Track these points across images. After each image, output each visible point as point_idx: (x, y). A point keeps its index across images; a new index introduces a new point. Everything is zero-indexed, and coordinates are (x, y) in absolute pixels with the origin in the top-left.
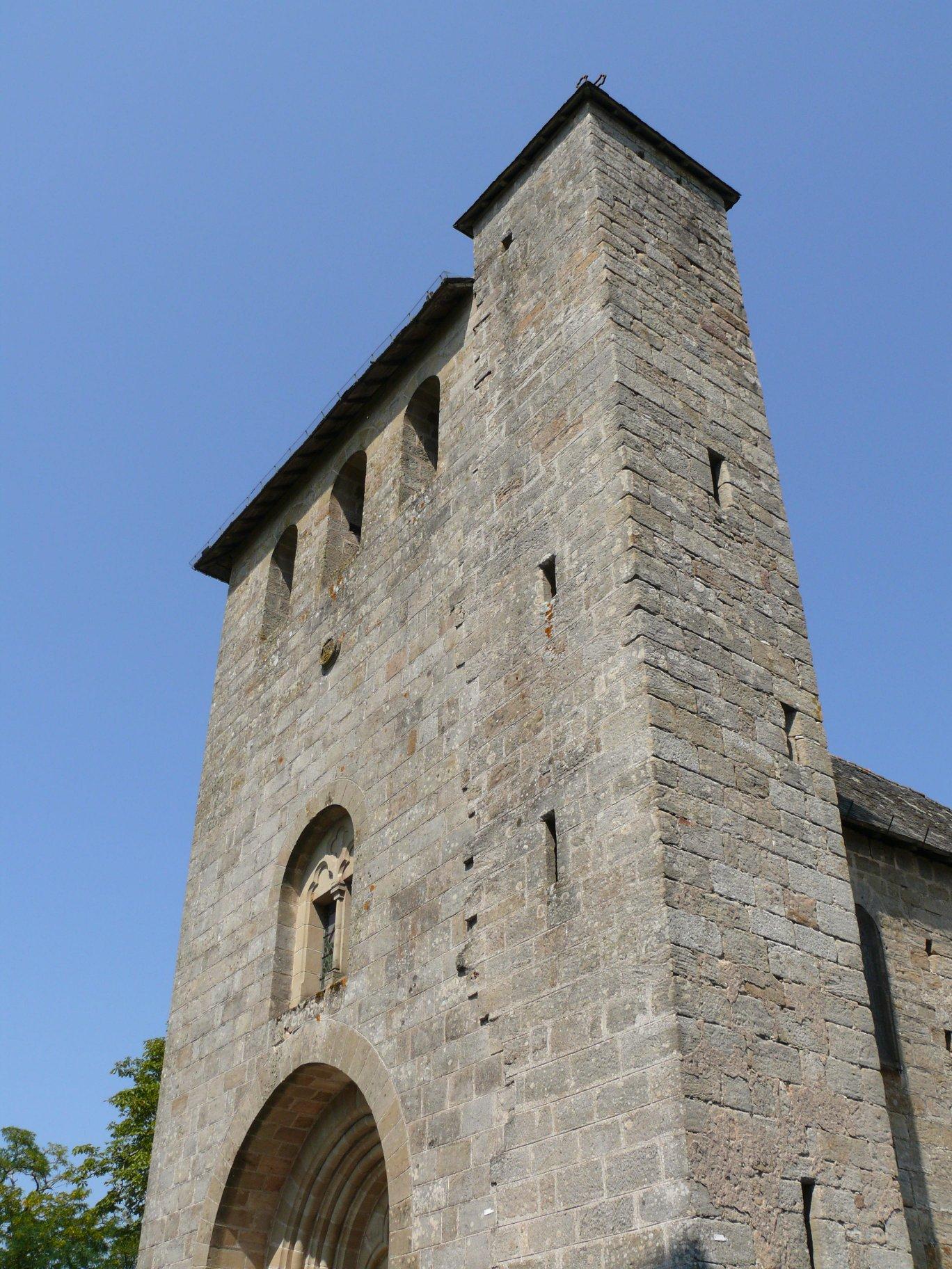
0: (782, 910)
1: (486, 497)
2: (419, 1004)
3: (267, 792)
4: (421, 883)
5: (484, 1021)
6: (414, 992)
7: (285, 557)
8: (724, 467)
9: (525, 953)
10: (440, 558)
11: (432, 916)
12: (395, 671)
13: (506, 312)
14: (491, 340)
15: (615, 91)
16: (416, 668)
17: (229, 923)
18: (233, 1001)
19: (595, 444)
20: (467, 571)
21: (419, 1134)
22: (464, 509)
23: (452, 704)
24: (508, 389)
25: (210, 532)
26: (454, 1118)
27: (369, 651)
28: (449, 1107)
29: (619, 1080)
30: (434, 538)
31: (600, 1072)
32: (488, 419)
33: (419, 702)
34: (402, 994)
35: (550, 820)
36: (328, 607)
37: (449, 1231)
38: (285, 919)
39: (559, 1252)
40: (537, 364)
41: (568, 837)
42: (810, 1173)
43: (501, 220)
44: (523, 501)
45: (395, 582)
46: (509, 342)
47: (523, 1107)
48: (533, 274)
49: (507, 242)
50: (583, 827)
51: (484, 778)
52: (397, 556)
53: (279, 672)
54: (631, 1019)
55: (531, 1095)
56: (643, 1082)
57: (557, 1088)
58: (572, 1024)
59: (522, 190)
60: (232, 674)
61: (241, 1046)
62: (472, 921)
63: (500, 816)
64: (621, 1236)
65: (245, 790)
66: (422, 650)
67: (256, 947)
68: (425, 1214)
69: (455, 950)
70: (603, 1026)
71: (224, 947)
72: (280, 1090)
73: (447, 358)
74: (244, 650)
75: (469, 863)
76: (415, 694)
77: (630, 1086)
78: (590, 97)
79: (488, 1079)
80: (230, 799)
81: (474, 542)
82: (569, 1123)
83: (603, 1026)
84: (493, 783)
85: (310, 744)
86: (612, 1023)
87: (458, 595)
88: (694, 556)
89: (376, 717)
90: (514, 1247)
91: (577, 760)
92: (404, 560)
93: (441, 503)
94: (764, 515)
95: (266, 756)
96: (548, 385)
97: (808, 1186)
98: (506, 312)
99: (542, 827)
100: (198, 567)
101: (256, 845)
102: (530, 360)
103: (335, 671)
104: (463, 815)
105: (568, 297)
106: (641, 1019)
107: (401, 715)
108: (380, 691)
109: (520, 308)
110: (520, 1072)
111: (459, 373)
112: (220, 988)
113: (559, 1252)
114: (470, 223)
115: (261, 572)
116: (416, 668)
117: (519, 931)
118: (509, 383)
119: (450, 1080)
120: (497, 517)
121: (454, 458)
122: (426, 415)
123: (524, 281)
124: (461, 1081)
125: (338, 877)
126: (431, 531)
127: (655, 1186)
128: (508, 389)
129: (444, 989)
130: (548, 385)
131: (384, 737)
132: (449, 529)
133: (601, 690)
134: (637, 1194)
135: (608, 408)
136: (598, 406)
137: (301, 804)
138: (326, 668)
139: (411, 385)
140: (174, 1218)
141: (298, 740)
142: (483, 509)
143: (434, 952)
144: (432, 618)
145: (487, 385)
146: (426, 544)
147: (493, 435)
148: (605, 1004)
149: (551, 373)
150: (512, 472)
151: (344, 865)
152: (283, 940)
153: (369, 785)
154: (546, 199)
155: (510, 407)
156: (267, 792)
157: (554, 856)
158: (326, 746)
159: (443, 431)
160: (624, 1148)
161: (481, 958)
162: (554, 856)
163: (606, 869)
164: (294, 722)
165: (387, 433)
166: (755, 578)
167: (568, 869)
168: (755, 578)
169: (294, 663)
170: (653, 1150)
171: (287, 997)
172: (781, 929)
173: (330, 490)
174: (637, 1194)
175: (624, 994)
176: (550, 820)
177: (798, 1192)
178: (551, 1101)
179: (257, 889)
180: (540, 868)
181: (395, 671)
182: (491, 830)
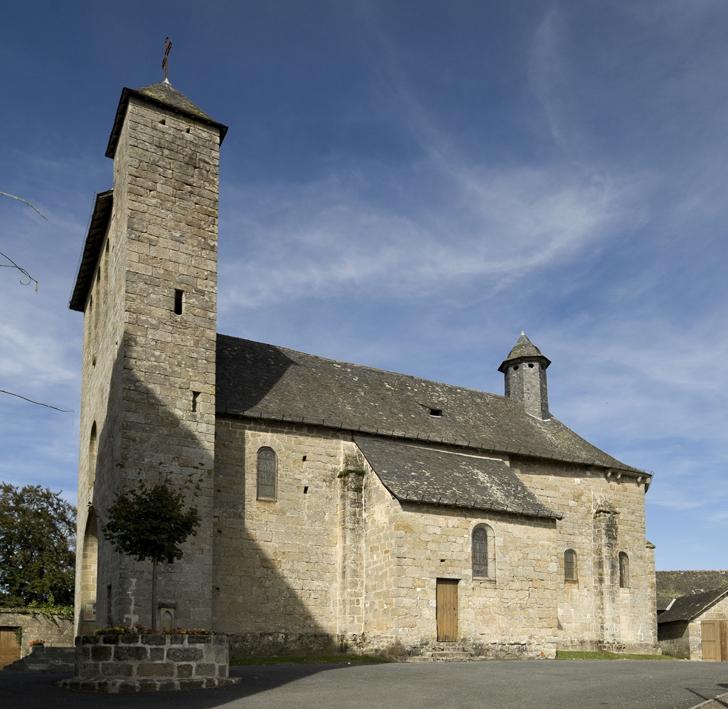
100: (71, 307)
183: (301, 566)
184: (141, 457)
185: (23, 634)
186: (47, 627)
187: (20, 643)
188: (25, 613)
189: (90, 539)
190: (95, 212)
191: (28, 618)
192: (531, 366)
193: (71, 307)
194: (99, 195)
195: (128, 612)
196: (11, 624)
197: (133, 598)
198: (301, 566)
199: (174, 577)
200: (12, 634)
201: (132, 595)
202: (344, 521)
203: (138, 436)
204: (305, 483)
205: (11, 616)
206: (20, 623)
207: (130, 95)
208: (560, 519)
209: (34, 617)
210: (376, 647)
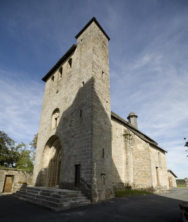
0: (104, 122)
1: (76, 73)
2: (66, 129)
3: (50, 106)
4: (67, 116)
5: (73, 131)
6: (65, 128)
7: (53, 79)
8: (104, 73)
9: (77, 124)
10: (71, 81)
11: (68, 120)
12: (65, 93)
13: (81, 50)
14: (79, 54)
15: (97, 20)
16: (67, 93)
17: (45, 120)
18: (46, 128)
19: (90, 68)
20: (74, 82)
21: (65, 142)
22: (74, 75)
23: (71, 98)
24: (80, 60)
25: (44, 75)
26: (69, 141)
27: (62, 91)
28: (68, 139)
29: (86, 137)
30: (70, 78)
31: (84, 137)
32: (78, 64)
33: (67, 97)
34: (64, 128)
35: (81, 111)
36: (57, 86)
37: (68, 152)
38: (52, 120)
39: (79, 154)
40: (84, 57)
41: (83, 112)
42: (104, 148)
43: (81, 37)
44: (81, 75)
45: (65, 83)
46: (81, 54)
47: (76, 140)
48: (84, 45)
49: (82, 40)
50: (84, 111)
51: (74, 106)
52: (66, 80)
53: (52, 93)
54: (88, 131)
55: (77, 139)
56: (88, 138)
57: (79, 138)
58: (82, 132)
59: (84, 33)
60: (46, 93)
61: (46, 133)
62: (72, 121)
63: (76, 110)
64: (85, 152)
65: (47, 106)
66: (68, 91)
67: (48, 123)
68: (65, 150)
69: (70, 124)
70: (85, 132)
71: (45, 123)
72: (51, 137)
73: (63, 65)
74: (48, 90)
75: (72, 115)
76: (67, 96)
77: (87, 138)
78: (94, 20)
79: (73, 137)
80: (46, 107)
81: (75, 79)
82: (80, 141)
83: (85, 132)
84: (75, 106)
85: (55, 101)
86: (86, 132)
87: (72, 85)
88: (99, 83)
89: (62, 98)
90: (74, 153)
91: (84, 104)
92: (66, 81)
93: (71, 74)
94: (107, 80)
95: (50, 102)
96: (85, 60)
97: (103, 149)
98: (81, 50)
99: (80, 111)
100: (42, 80)
101: (48, 112)
102: (83, 57)
103: (58, 93)
104: (71, 110)
105: (89, 48)
106: (89, 131)
107: (65, 98)
108: (63, 96)
109: (82, 50)
110: (76, 136)
111: (74, 57)
112: (44, 127)
113: (79, 154)
114: (77, 37)
115: (50, 80)
116: (67, 93)
117: (77, 122)
118: (80, 60)
119: (68, 137)
120: (78, 76)
121: (73, 69)
122: (70, 63)
123: (83, 46)
124: (69, 137)
125: (58, 116)
126: (70, 78)
127: (89, 148)
128: (80, 60)
129: (68, 128)
130: (85, 60)
131: (63, 101)
132: (72, 77)
133: (88, 97)
134: (87, 149)
135: (92, 64)
136: (91, 63)
137: (54, 108)
138: (57, 93)
139: (60, 67)
140: (39, 150)
141: (54, 101)
142: (76, 75)
143: (68, 124)
144: (69, 88)
145: (77, 60)
146: (69, 79)
147: (78, 66)
148: (85, 130)
149: (85, 58)
150: (80, 71)
151: (58, 114)
152: (51, 122)
153: (61, 106)
154: (87, 34)
155: (80, 63)
156: (50, 106)
157: (81, 114)
158: (57, 101)
159: (72, 65)
160: (86, 144)
161: (73, 125)
162: (81, 114)
163: (86, 116)
164: (53, 99)
165: (57, 72)
166: (105, 87)
167: (82, 116)
168: (105, 87)
169: (53, 92)
170: (89, 144)
171: (51, 128)
172: (104, 124)
173: (51, 78)
174: (87, 149)
175: (87, 129)
176: (81, 111)
177: (102, 150)
178: (79, 139)
179: (49, 117)
180: (80, 116)
181: (65, 93)
182: (74, 111)
183: (118, 161)
184: (96, 118)
185: (14, 178)
186: (22, 176)
187: (13, 182)
188: (16, 170)
189: (47, 146)
190: (72, 47)
191: (17, 172)
192: (132, 118)
193: (42, 80)
194: (74, 45)
195: (94, 177)
196: (11, 174)
197: (95, 171)
198: (118, 161)
199: (105, 163)
200: (10, 178)
201: (95, 170)
202: (126, 148)
203: (96, 110)
204: (117, 136)
205: (11, 171)
206: (14, 174)
207: (94, 20)
208: (167, 152)
209: (19, 172)
210: (141, 188)
